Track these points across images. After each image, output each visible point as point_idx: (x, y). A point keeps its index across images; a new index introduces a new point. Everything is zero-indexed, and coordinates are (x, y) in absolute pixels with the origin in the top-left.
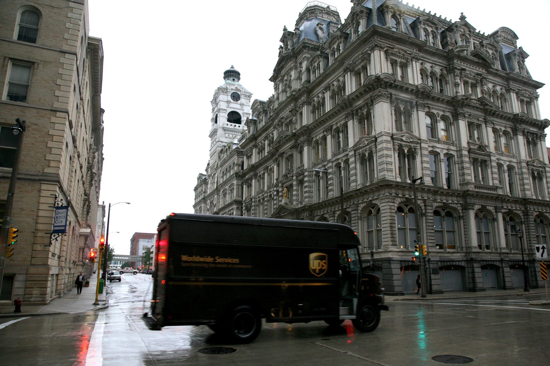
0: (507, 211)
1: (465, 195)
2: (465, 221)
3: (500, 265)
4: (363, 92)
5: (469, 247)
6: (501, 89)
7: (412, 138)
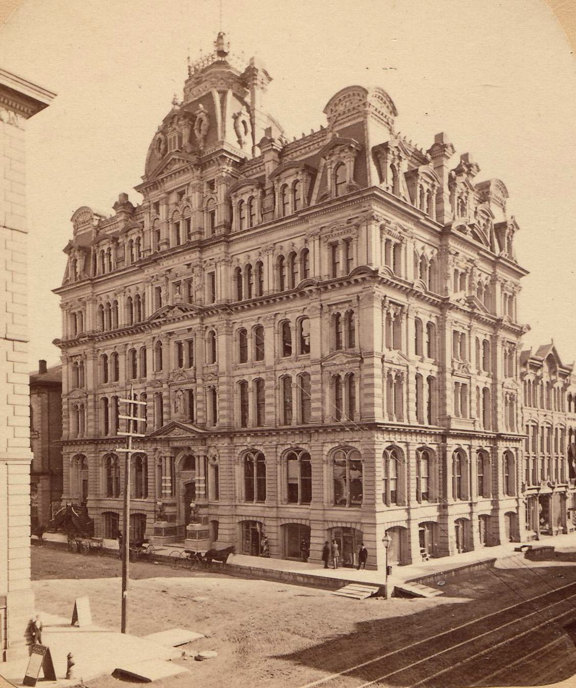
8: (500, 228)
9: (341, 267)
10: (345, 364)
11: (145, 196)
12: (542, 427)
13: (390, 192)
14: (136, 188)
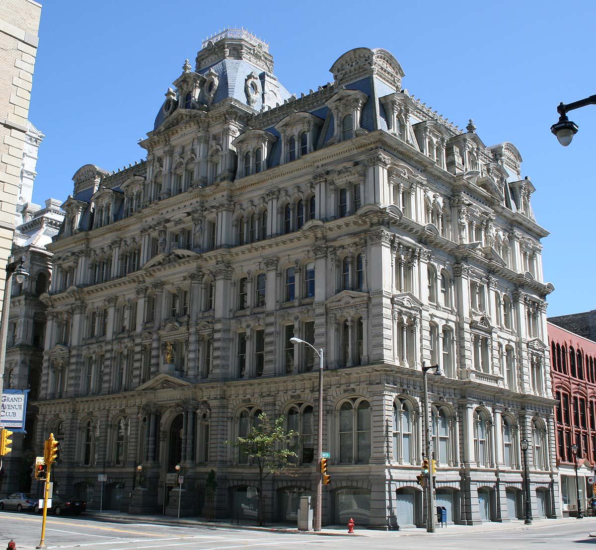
8: (514, 190)
11: (149, 151)
12: (575, 398)
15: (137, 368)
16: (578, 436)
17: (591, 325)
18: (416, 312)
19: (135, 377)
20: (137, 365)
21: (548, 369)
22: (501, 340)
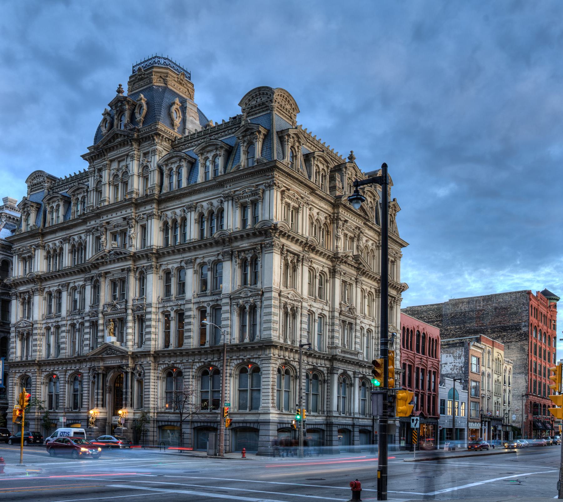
0: (312, 367)
1: (333, 359)
2: (329, 385)
3: (352, 430)
4: (251, 234)
5: (329, 411)
6: (372, 244)
7: (296, 296)
9: (249, 222)
10: (249, 297)
13: (289, 166)
14: (83, 156)
15: (87, 339)
16: (429, 397)
17: (443, 313)
18: (297, 303)
19: (86, 345)
20: (87, 336)
21: (398, 346)
22: (363, 325)
